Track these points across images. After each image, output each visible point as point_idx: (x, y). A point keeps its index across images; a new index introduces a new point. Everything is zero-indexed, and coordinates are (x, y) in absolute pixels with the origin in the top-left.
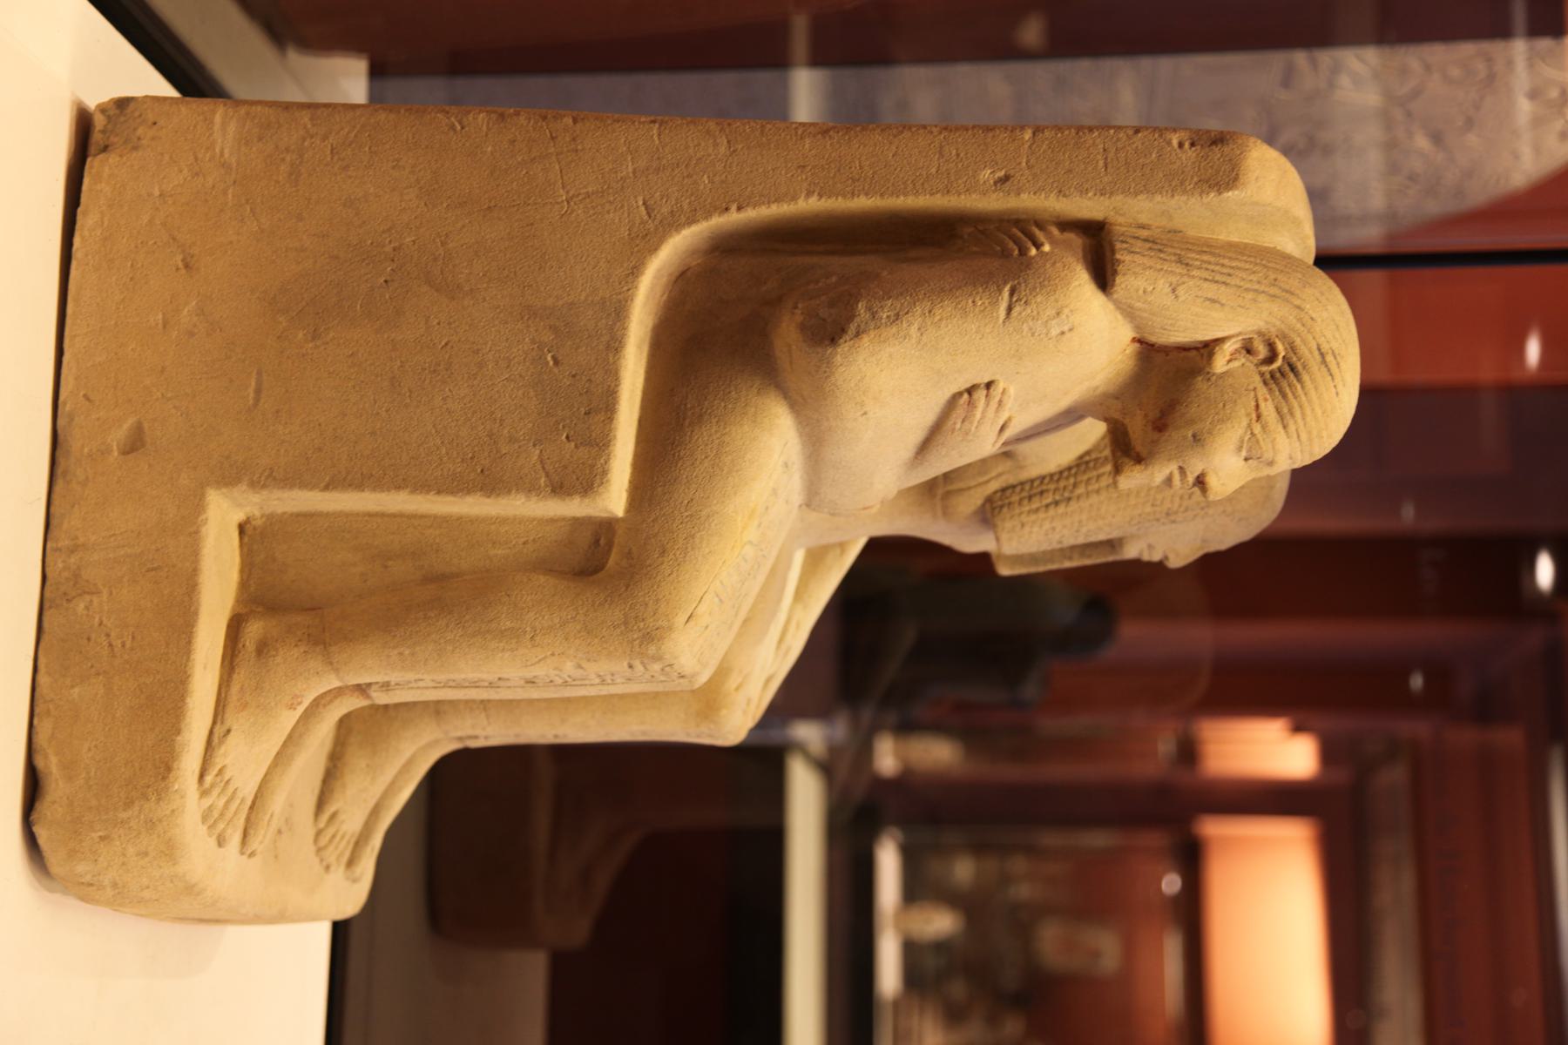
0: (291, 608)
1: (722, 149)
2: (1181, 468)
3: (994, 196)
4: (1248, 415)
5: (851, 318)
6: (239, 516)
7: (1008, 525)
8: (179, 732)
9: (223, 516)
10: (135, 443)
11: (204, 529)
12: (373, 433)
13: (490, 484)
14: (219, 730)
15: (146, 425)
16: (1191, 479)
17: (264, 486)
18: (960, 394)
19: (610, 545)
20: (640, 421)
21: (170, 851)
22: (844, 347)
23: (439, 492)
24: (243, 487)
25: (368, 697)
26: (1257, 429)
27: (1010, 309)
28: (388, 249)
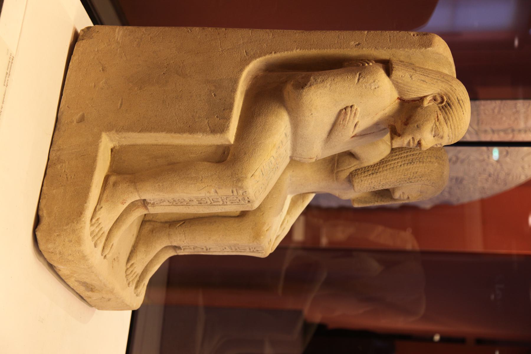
0: (126, 171)
1: (271, 37)
2: (413, 138)
3: (355, 49)
4: (435, 119)
5: (309, 81)
6: (111, 145)
7: (357, 181)
8: (86, 203)
9: (106, 144)
10: (82, 120)
11: (100, 144)
12: (156, 116)
13: (191, 130)
14: (98, 207)
15: (85, 115)
16: (416, 142)
17: (120, 131)
18: (342, 110)
19: (228, 154)
20: (240, 116)
21: (79, 241)
22: (306, 89)
23: (175, 133)
24: (114, 132)
25: (147, 209)
26: (438, 124)
27: (359, 80)
28: (166, 64)
